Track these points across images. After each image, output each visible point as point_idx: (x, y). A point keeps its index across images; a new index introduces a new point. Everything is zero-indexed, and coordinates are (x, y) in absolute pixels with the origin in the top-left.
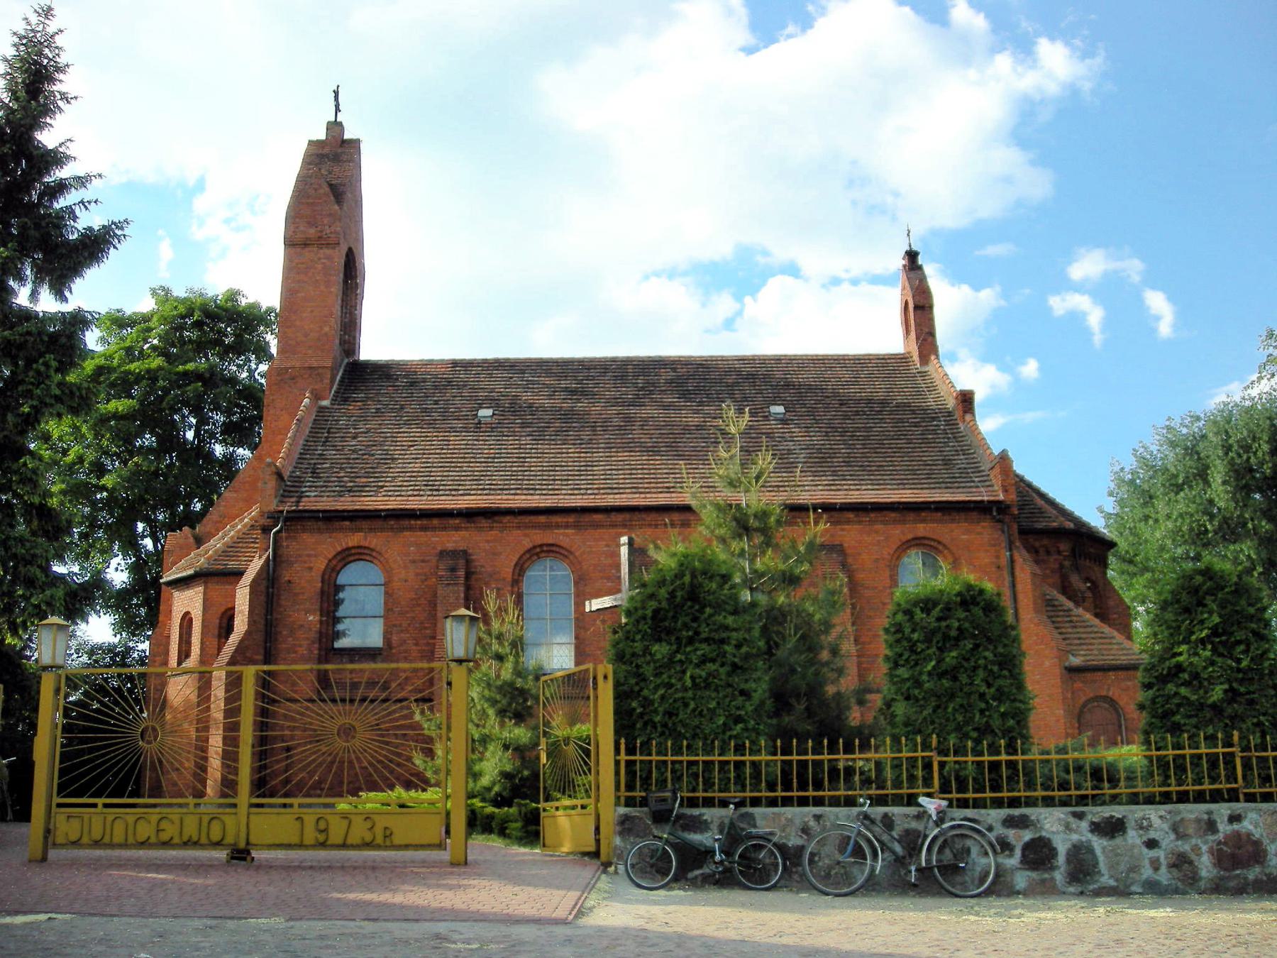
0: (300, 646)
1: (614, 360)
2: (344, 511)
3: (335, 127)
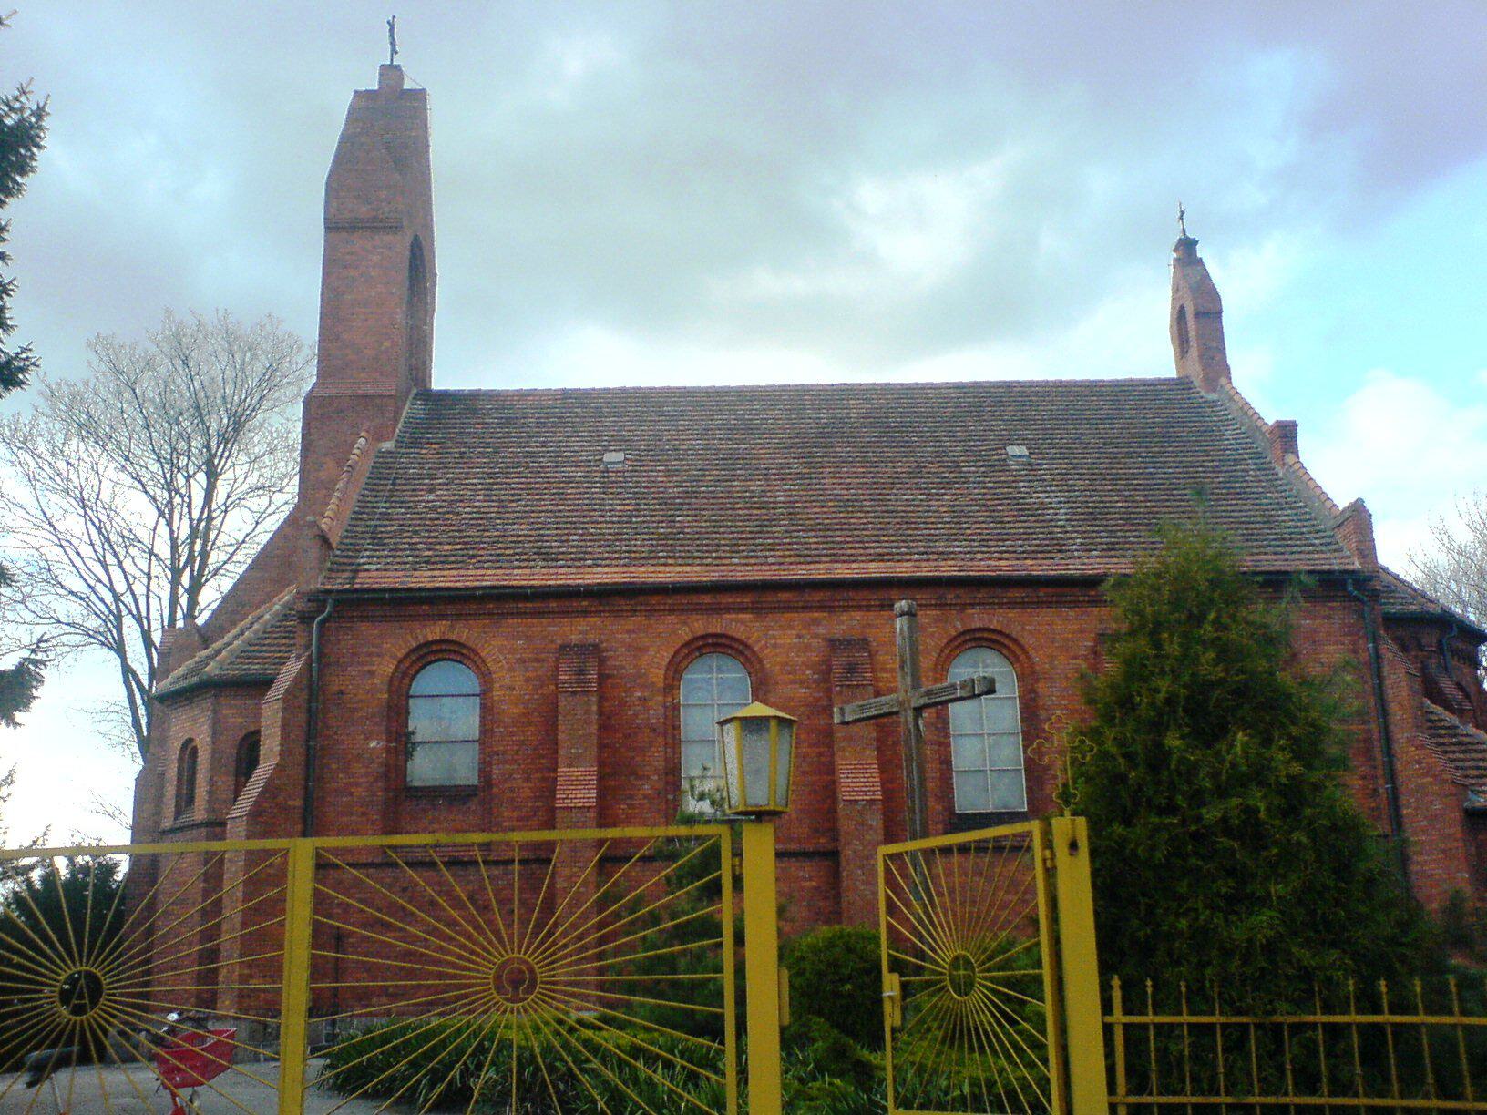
0: (358, 785)
1: (785, 388)
2: (420, 590)
3: (391, 72)
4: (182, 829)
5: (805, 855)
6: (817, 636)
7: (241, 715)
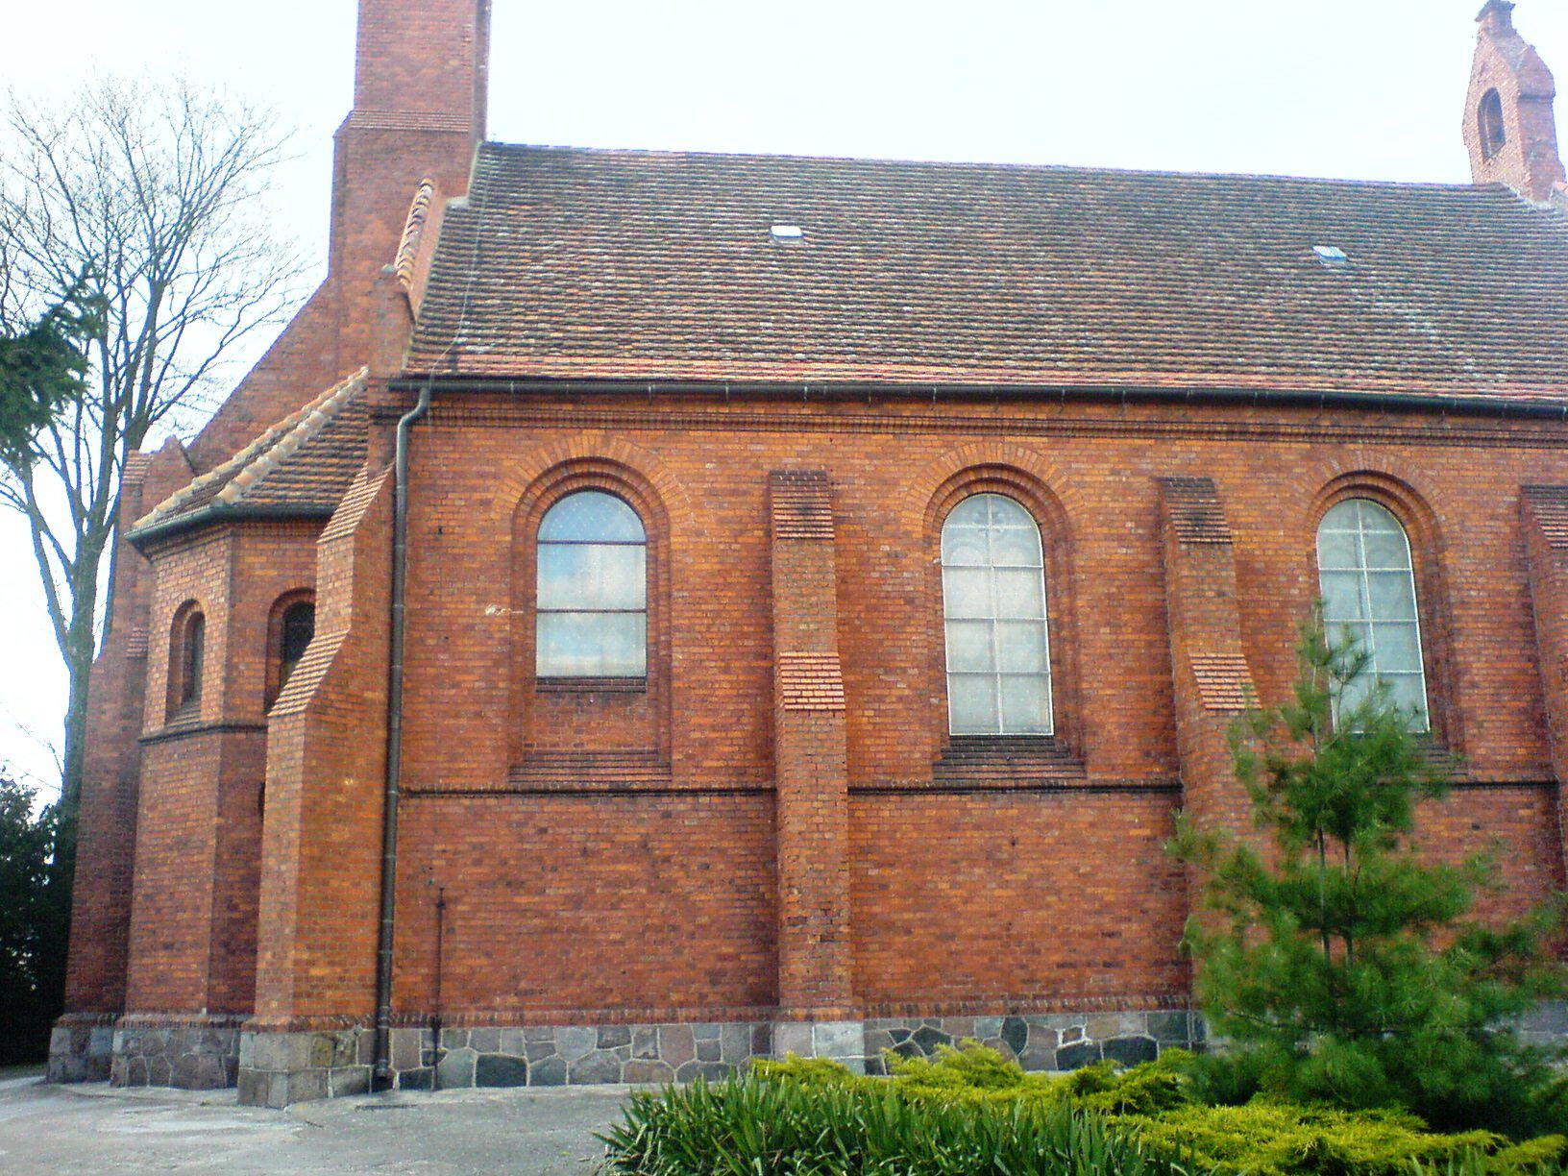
0: (467, 671)
4: (179, 735)
5: (1134, 789)
6: (1139, 473)
7: (274, 565)
